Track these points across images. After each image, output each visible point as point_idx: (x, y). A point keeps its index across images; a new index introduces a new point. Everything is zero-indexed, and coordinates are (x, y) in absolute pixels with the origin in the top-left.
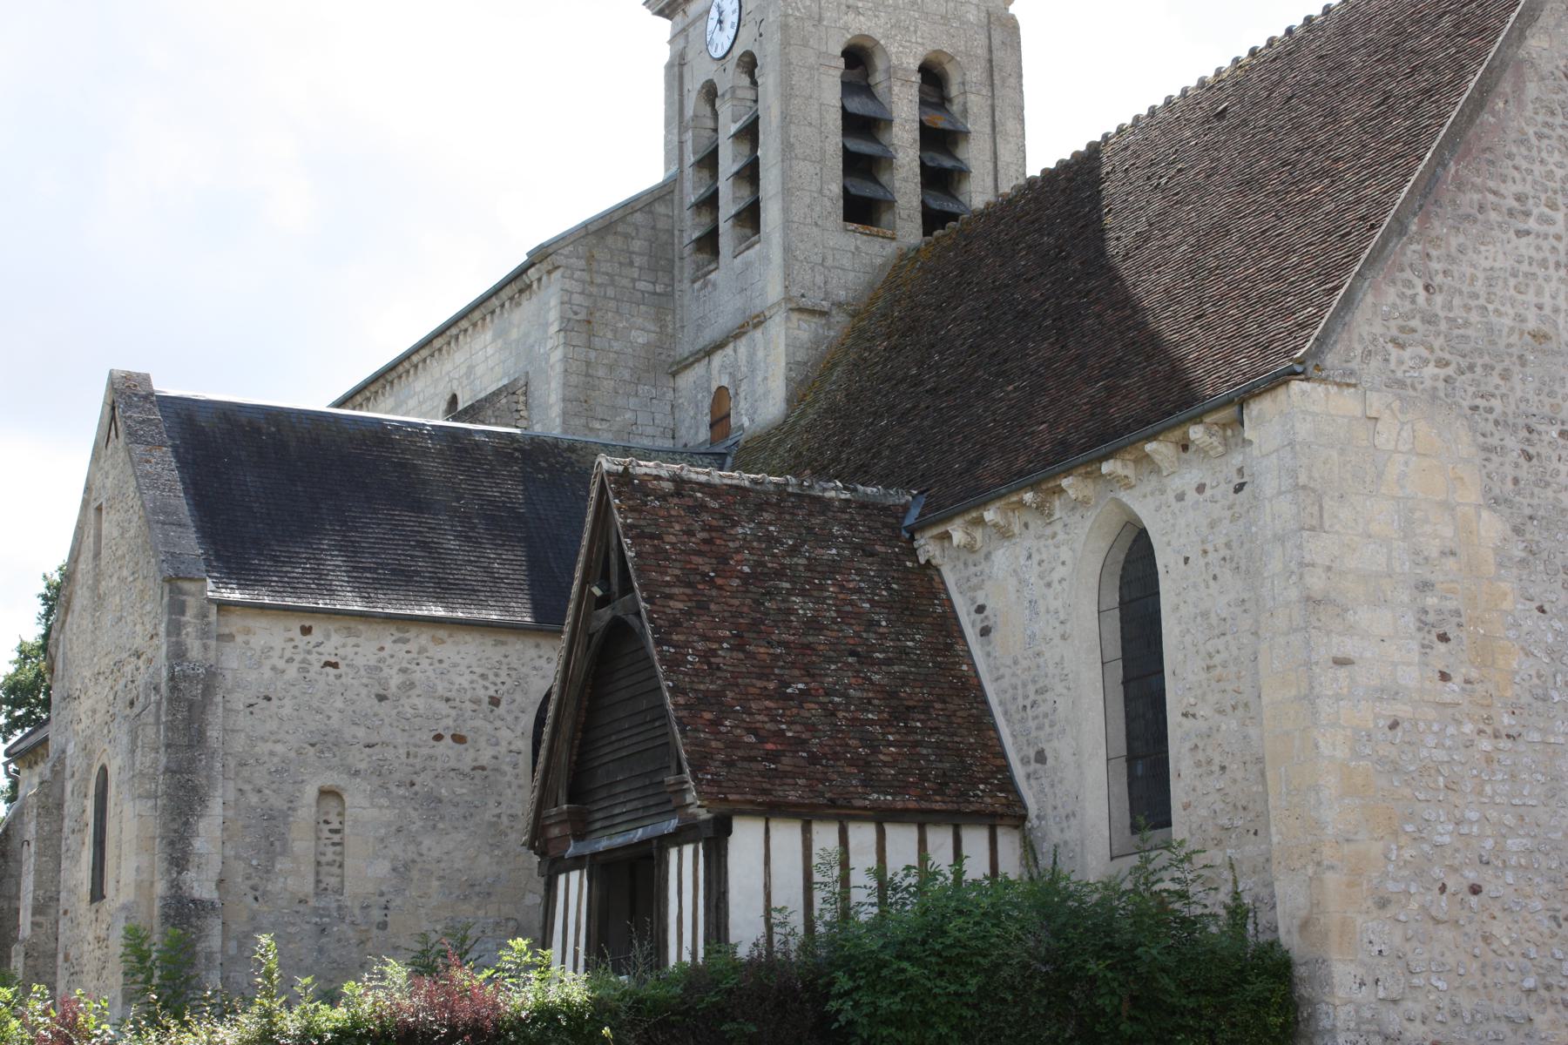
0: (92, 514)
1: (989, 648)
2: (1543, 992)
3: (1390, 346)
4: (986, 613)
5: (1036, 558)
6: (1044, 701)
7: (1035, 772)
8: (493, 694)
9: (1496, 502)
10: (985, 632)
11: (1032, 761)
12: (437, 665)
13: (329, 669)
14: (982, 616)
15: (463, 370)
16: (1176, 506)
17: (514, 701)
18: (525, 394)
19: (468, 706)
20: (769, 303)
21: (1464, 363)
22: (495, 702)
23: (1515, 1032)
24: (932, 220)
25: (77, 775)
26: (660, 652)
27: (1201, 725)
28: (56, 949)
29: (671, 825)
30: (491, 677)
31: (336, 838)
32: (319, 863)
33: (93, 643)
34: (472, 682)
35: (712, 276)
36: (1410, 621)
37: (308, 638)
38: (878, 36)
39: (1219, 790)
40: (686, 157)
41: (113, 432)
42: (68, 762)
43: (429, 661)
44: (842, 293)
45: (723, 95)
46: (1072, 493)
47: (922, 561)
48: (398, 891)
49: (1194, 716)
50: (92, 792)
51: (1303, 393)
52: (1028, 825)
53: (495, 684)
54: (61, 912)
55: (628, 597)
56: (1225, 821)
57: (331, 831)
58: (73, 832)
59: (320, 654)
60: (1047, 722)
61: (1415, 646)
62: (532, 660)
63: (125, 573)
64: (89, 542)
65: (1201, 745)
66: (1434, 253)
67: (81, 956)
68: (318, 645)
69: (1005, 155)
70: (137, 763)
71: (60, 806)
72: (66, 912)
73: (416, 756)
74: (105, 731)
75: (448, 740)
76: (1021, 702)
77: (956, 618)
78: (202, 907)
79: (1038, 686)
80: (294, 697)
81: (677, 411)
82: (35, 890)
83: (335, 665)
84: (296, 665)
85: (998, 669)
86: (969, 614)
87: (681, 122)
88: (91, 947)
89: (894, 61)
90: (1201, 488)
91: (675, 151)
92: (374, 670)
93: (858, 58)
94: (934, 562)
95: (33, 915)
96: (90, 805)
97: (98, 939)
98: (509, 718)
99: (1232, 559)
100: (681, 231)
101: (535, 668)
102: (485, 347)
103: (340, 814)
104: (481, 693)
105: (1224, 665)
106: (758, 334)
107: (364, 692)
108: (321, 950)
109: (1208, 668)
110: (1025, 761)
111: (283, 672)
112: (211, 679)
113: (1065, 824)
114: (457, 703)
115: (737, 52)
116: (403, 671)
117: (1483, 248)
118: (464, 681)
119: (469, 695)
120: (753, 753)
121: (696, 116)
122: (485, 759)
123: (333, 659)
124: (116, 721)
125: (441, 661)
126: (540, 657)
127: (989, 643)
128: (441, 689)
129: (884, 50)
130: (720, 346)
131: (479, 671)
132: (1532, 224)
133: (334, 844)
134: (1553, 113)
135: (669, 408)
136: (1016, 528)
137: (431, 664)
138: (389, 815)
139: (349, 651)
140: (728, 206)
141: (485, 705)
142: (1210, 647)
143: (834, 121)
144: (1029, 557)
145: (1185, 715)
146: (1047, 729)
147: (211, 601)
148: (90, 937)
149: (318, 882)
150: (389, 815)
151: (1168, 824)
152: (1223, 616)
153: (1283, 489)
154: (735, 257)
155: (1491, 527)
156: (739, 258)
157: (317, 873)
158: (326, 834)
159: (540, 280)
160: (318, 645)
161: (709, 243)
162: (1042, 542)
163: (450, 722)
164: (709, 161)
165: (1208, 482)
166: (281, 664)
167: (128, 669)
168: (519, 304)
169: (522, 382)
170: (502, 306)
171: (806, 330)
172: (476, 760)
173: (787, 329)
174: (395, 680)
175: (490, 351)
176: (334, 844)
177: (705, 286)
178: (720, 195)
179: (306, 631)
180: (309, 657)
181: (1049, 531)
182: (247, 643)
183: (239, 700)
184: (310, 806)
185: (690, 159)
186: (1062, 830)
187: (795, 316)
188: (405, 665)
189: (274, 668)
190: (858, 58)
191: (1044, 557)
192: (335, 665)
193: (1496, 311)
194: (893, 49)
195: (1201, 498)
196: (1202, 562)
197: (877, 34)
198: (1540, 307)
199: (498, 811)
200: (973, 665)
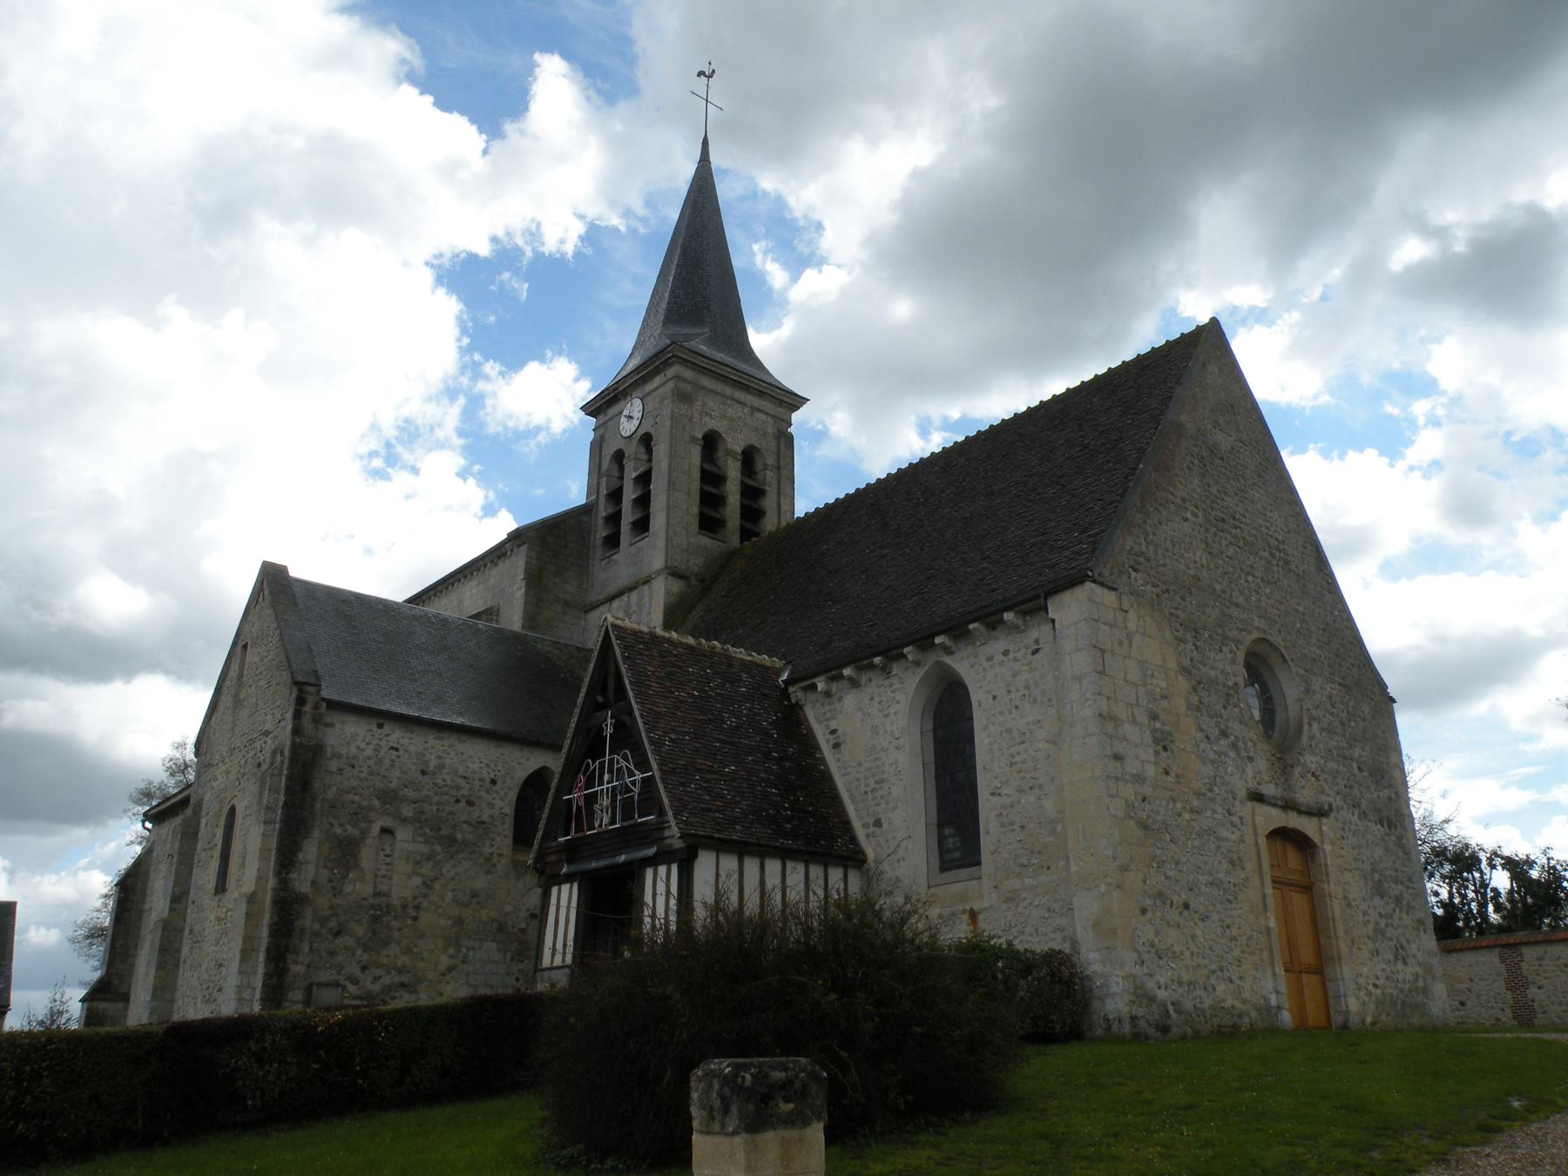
0: (239, 649)
1: (840, 756)
2: (1219, 973)
3: (1130, 569)
4: (837, 734)
5: (877, 699)
6: (881, 788)
7: (873, 833)
8: (493, 777)
9: (1184, 670)
10: (836, 746)
11: (871, 826)
12: (459, 755)
13: (393, 752)
14: (834, 736)
15: (455, 603)
16: (986, 665)
17: (505, 782)
18: (497, 615)
19: (477, 783)
20: (654, 570)
21: (1164, 588)
22: (494, 782)
23: (1208, 997)
24: (746, 534)
25: (210, 814)
26: (649, 737)
27: (1006, 801)
28: (184, 926)
29: (651, 851)
30: (493, 766)
31: (388, 860)
32: (376, 876)
33: (232, 729)
34: (481, 768)
35: (615, 557)
36: (1148, 736)
37: (380, 731)
38: (722, 432)
39: (1020, 841)
40: (601, 490)
41: (261, 598)
42: (205, 806)
43: (455, 753)
44: (696, 568)
45: (629, 457)
46: (910, 657)
47: (793, 701)
48: (425, 896)
49: (999, 795)
50: (222, 823)
51: (1092, 589)
52: (866, 866)
53: (494, 771)
54: (190, 902)
55: (622, 703)
56: (1024, 861)
57: (385, 855)
58: (205, 850)
59: (388, 741)
60: (883, 801)
61: (1151, 751)
62: (518, 758)
63: (262, 683)
64: (235, 667)
65: (1005, 813)
66: (1148, 521)
67: (204, 930)
68: (387, 736)
69: (784, 507)
70: (265, 800)
71: (196, 833)
72: (193, 902)
73: (443, 811)
74: (237, 784)
75: (462, 804)
76: (863, 789)
77: (815, 738)
78: (303, 900)
79: (876, 779)
80: (369, 767)
81: (586, 633)
82: (173, 887)
83: (397, 749)
84: (372, 747)
85: (846, 769)
86: (824, 735)
87: (599, 472)
88: (213, 924)
89: (729, 446)
90: (1006, 653)
91: (593, 488)
92: (420, 755)
93: (711, 442)
94: (800, 703)
95: (171, 903)
96: (220, 833)
97: (218, 919)
98: (502, 793)
99: (1030, 696)
100: (595, 532)
101: (519, 764)
102: (472, 589)
103: (391, 845)
104: (485, 775)
105: (1024, 762)
106: (646, 588)
107: (413, 767)
108: (374, 932)
109: (1011, 763)
110: (866, 826)
111: (363, 750)
112: (317, 751)
113: (896, 865)
114: (471, 780)
115: (640, 433)
116: (440, 757)
117: (1169, 523)
118: (475, 767)
119: (478, 776)
120: (710, 806)
121: (607, 470)
122: (485, 818)
123: (396, 746)
124: (246, 777)
125: (462, 753)
126: (522, 757)
127: (840, 753)
128: (461, 770)
129: (724, 439)
130: (619, 594)
131: (485, 761)
132: (1189, 515)
133: (387, 864)
134: (1193, 457)
135: (581, 631)
136: (863, 682)
137: (456, 755)
138: (424, 848)
139: (406, 741)
140: (628, 515)
141: (488, 783)
142: (1012, 750)
143: (696, 474)
144: (872, 699)
145: (993, 794)
146: (883, 805)
147: (324, 699)
148: (212, 917)
149: (375, 887)
150: (424, 848)
151: (979, 863)
152: (1023, 731)
153: (1080, 647)
154: (631, 545)
155: (1183, 684)
156: (634, 546)
157: (375, 882)
158: (382, 857)
159: (512, 550)
160: (387, 736)
161: (613, 541)
162: (882, 689)
163: (465, 792)
164: (616, 496)
165: (1011, 649)
166: (363, 745)
167: (258, 744)
168: (496, 565)
169: (496, 608)
170: (486, 566)
171: (677, 586)
172: (479, 817)
173: (666, 584)
174: (433, 763)
175: (474, 591)
176: (387, 864)
177: (609, 563)
178: (623, 511)
179: (380, 726)
180: (381, 743)
181: (887, 682)
182: (342, 729)
183: (333, 765)
184: (374, 838)
185: (604, 492)
186: (894, 869)
187: (670, 578)
188: (440, 754)
189: (358, 747)
190: (711, 442)
191: (883, 698)
192: (397, 749)
193: (1177, 560)
194: (729, 440)
195: (1006, 659)
196: (1007, 699)
197: (721, 430)
198: (1195, 562)
199: (491, 851)
200: (826, 765)
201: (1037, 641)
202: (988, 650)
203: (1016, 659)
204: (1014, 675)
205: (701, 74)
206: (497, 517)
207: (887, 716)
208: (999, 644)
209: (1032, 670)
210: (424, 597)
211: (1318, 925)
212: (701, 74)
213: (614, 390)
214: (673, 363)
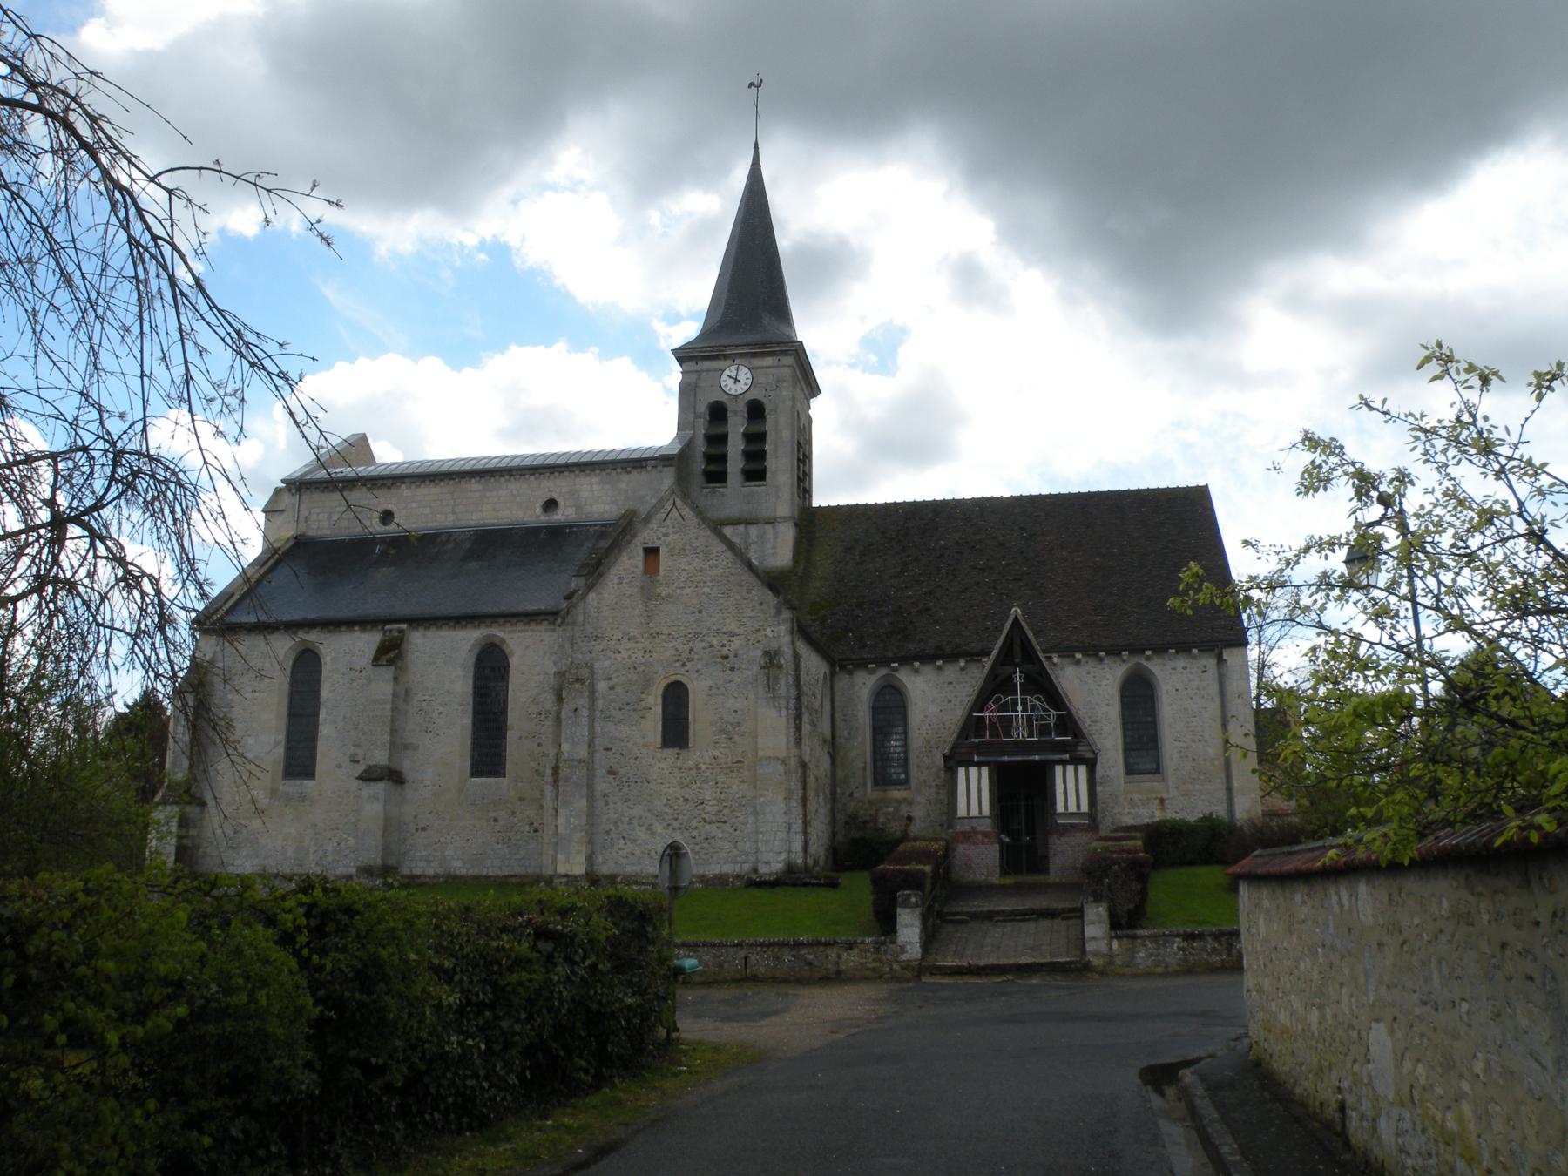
5: (1092, 674)
27: (1184, 745)
56: (1195, 776)
90: (1185, 668)
105: (1196, 727)
115: (749, 397)
181: (1100, 666)
197: (760, 397)
201: (1205, 667)
202: (1173, 664)
203: (1191, 673)
204: (1190, 681)
205: (751, 85)
206: (416, 362)
207: (1100, 685)
208: (1181, 662)
209: (1201, 681)
210: (514, 473)
211: (800, 735)
212: (751, 85)
213: (720, 351)
214: (790, 355)
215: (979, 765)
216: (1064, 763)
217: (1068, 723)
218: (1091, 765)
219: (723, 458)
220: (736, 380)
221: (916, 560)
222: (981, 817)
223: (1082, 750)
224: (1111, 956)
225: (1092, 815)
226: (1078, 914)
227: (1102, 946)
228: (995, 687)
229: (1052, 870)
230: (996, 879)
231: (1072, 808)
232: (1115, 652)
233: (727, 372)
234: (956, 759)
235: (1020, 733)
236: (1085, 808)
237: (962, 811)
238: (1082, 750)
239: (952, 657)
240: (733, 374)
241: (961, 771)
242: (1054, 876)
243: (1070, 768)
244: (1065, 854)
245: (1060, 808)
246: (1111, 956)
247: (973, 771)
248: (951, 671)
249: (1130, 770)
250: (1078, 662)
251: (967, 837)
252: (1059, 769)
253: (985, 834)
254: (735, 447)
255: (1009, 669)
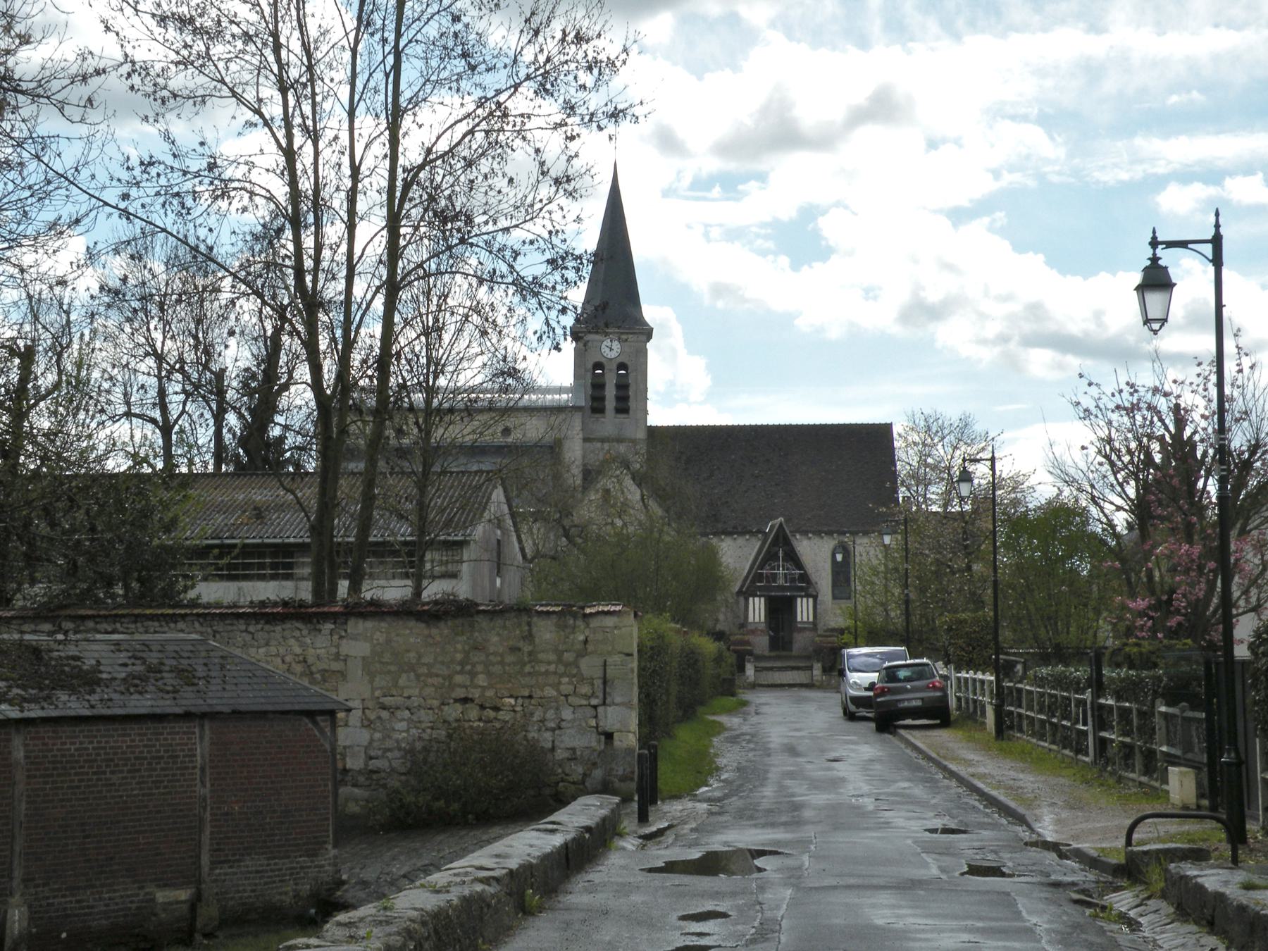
115: (620, 360)
215: (760, 596)
216: (802, 597)
217: (805, 578)
218: (815, 598)
219: (603, 399)
220: (611, 349)
221: (718, 468)
222: (760, 622)
223: (811, 591)
224: (822, 681)
225: (815, 623)
226: (810, 668)
227: (819, 678)
228: (768, 558)
229: (794, 649)
230: (767, 653)
231: (805, 619)
232: (830, 533)
233: (605, 343)
234: (747, 593)
235: (781, 582)
236: (811, 619)
237: (751, 619)
238: (811, 591)
239: (742, 534)
240: (609, 344)
241: (751, 599)
242: (795, 652)
243: (805, 600)
244: (801, 642)
245: (799, 619)
246: (822, 681)
247: (757, 599)
248: (741, 541)
249: (835, 597)
250: (810, 538)
251: (753, 632)
252: (799, 600)
253: (762, 631)
254: (610, 392)
255: (776, 549)
